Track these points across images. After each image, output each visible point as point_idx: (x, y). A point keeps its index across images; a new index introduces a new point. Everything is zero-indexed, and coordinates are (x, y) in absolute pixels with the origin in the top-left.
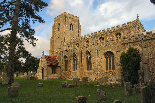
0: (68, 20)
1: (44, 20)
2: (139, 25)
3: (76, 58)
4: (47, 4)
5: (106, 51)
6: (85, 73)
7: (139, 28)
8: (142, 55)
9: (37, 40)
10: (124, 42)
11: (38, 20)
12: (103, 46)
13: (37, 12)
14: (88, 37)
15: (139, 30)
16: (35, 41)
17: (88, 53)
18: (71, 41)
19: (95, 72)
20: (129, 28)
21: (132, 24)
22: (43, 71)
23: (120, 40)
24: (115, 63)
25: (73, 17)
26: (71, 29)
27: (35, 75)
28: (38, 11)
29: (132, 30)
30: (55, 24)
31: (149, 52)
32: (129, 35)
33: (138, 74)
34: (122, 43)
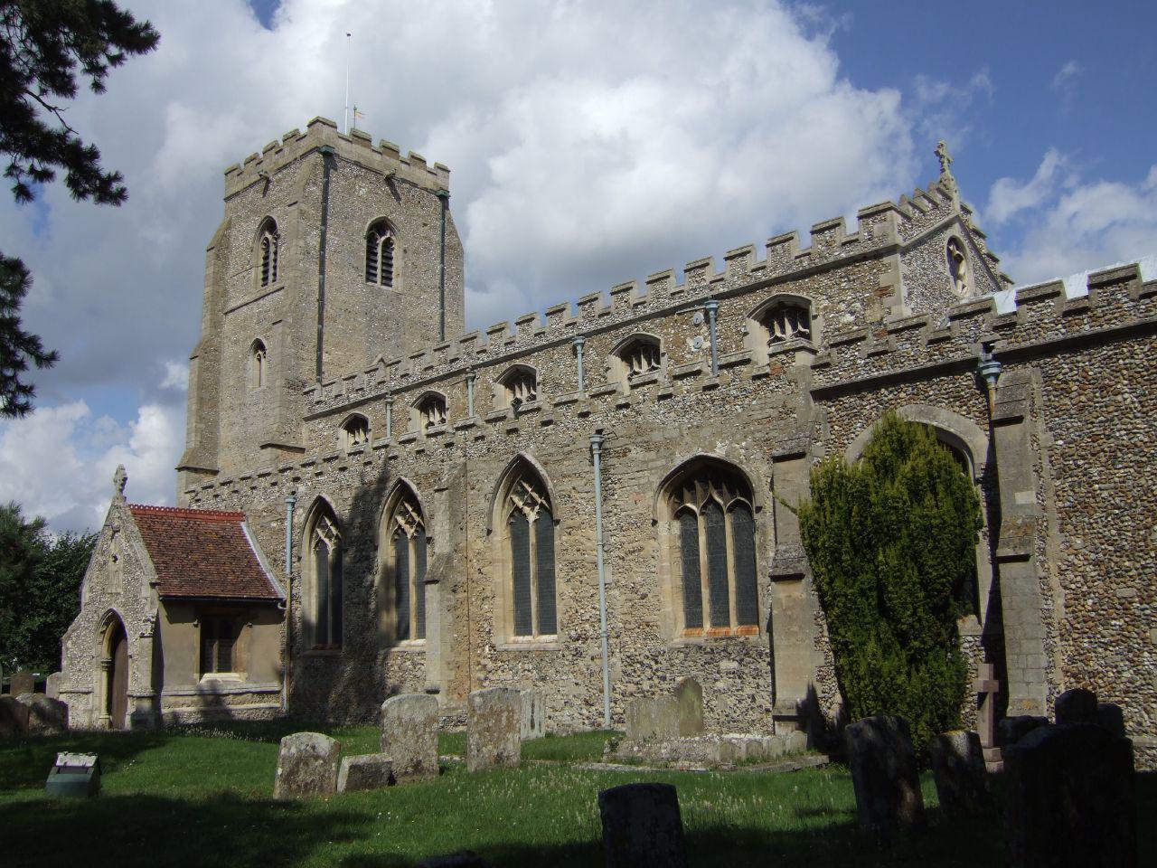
0: (350, 191)
1: (117, 178)
2: (956, 231)
3: (421, 529)
4: (147, 26)
5: (680, 459)
6: (497, 655)
7: (955, 261)
8: (990, 479)
9: (53, 357)
10: (841, 377)
11: (61, 172)
12: (655, 414)
13: (52, 98)
14: (523, 340)
15: (957, 277)
16: (30, 362)
17: (522, 474)
18: (379, 376)
19: (592, 648)
20: (877, 255)
21: (899, 219)
22: (119, 655)
23: (803, 359)
24: (765, 563)
25: (394, 162)
26: (379, 272)
27: (40, 687)
28: (65, 87)
29: (903, 269)
30: (229, 225)
31: (1045, 454)
32: (873, 314)
33: (957, 646)
34: (821, 381)
